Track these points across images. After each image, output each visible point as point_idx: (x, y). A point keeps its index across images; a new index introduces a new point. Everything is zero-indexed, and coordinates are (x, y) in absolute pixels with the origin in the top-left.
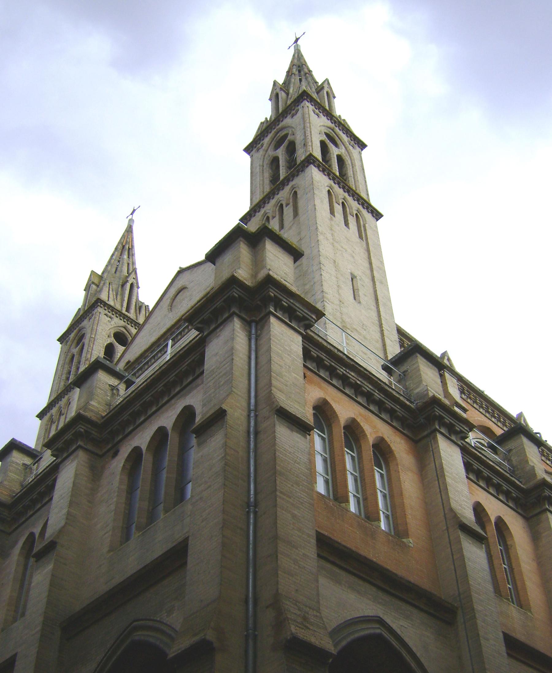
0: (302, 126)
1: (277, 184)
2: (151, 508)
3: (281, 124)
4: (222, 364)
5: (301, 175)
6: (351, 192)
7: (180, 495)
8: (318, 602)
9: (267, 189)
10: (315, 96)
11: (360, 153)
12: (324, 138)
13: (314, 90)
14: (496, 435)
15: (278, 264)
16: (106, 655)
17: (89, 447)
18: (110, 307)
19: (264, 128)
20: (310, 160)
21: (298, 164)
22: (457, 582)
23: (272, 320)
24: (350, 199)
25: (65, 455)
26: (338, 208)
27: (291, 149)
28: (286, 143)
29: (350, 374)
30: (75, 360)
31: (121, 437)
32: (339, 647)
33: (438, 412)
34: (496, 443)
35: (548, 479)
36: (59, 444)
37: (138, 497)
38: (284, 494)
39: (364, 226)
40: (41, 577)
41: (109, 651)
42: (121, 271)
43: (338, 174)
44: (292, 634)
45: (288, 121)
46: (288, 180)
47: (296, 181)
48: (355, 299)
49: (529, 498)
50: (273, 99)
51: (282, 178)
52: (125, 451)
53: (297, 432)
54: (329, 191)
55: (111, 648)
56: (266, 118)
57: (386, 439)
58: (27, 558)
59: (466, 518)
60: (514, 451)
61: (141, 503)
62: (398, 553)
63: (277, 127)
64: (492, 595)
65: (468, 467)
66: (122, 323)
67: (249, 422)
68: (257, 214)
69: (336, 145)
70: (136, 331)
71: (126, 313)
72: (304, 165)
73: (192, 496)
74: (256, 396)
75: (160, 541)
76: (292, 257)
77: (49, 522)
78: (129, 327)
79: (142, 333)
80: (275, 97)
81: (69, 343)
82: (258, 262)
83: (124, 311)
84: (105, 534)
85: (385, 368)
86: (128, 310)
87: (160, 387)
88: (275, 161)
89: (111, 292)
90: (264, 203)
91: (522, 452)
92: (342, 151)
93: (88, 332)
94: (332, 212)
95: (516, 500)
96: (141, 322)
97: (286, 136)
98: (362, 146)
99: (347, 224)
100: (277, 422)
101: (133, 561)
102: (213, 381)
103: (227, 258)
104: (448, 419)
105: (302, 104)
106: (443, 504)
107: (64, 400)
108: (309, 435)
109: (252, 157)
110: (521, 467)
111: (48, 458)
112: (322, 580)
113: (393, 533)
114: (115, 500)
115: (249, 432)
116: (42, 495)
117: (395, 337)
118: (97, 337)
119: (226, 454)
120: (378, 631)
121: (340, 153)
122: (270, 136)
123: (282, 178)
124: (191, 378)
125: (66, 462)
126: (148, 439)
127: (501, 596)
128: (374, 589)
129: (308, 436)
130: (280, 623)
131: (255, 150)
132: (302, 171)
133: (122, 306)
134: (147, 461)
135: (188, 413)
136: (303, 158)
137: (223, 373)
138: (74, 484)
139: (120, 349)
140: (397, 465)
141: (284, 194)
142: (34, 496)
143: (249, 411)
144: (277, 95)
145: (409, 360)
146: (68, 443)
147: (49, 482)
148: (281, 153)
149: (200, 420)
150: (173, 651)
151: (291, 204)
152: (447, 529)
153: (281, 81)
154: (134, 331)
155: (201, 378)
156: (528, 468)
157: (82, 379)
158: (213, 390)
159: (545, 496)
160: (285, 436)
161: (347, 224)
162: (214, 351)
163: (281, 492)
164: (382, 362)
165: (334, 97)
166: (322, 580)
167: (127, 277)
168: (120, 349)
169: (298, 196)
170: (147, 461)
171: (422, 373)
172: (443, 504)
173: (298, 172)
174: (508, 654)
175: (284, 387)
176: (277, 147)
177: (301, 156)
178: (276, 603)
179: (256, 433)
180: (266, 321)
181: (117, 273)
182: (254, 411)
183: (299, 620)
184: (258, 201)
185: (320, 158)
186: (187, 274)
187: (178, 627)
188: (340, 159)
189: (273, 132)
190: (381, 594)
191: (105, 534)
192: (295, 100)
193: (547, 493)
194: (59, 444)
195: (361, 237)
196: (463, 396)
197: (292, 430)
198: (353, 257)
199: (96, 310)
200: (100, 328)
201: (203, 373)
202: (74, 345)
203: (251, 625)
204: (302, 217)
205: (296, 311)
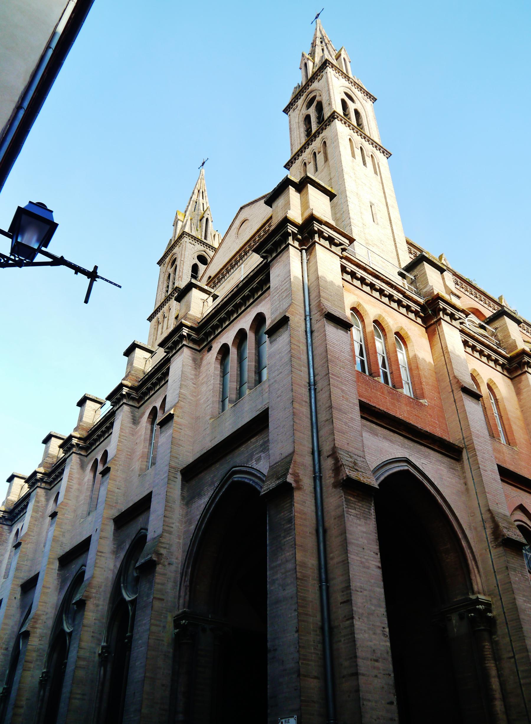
0: (327, 88)
1: (311, 137)
2: (238, 387)
3: (311, 88)
4: (283, 283)
5: (328, 128)
6: (367, 138)
7: (259, 380)
8: (364, 451)
9: (303, 141)
10: (335, 62)
13: (334, 57)
14: (484, 316)
15: (320, 205)
16: (214, 492)
17: (191, 345)
18: (192, 237)
19: (297, 92)
20: (333, 116)
21: (325, 119)
22: (462, 429)
23: (317, 246)
25: (174, 352)
26: (358, 152)
27: (320, 108)
28: (315, 103)
30: (171, 278)
31: (212, 337)
32: (379, 481)
33: (442, 305)
34: (485, 323)
35: (527, 349)
36: (170, 344)
37: (229, 379)
38: (335, 376)
39: (378, 164)
40: (164, 438)
41: (216, 488)
42: (199, 209)
43: (356, 125)
44: (347, 476)
45: (315, 85)
46: (318, 133)
47: (325, 133)
49: (513, 365)
51: (313, 132)
52: (216, 346)
53: (341, 329)
54: (350, 139)
55: (218, 487)
57: (404, 328)
58: (152, 423)
59: (465, 382)
60: (499, 329)
61: (232, 384)
62: (417, 410)
63: (307, 91)
64: (488, 437)
65: (465, 343)
66: (202, 248)
67: (306, 324)
68: (297, 161)
70: (214, 253)
71: (205, 241)
72: (330, 120)
73: (269, 380)
74: (310, 305)
75: (247, 413)
77: (167, 400)
78: (208, 251)
79: (217, 255)
81: (166, 265)
82: (305, 204)
83: (203, 240)
84: (207, 406)
85: (401, 274)
86: (205, 238)
88: (308, 118)
89: (192, 225)
90: (302, 152)
91: (505, 329)
93: (178, 256)
94: (353, 156)
95: (503, 366)
96: (217, 247)
97: (314, 97)
99: (365, 164)
100: (326, 324)
101: (229, 426)
102: (278, 295)
103: (280, 202)
104: (450, 310)
105: (325, 71)
106: (448, 373)
107: (166, 308)
108: (350, 331)
110: (504, 341)
111: (161, 353)
112: (365, 434)
113: (412, 397)
114: (212, 382)
115: (306, 331)
116: (159, 380)
117: (405, 246)
118: (186, 259)
119: (291, 349)
120: (406, 468)
122: (303, 98)
123: (313, 132)
124: (260, 293)
125: (175, 356)
126: (233, 338)
127: (494, 437)
128: (402, 438)
129: (349, 332)
130: (337, 468)
131: (291, 110)
132: (329, 125)
133: (201, 236)
134: (233, 352)
135: (260, 319)
136: (329, 114)
137: (284, 289)
138: (182, 372)
139: (202, 267)
140: (413, 346)
141: (316, 144)
142: (154, 380)
143: (306, 316)
145: (418, 267)
146: (176, 343)
147: (164, 370)
148: (312, 111)
149: (271, 323)
150: (264, 489)
151: (322, 152)
152: (452, 391)
154: (211, 253)
155: (267, 292)
156: (511, 341)
157: (182, 294)
158: (278, 302)
159: (525, 362)
160: (333, 333)
161: (365, 164)
162: (276, 274)
163: (333, 374)
164: (398, 270)
166: (365, 434)
167: (204, 213)
168: (202, 267)
169: (327, 145)
170: (233, 352)
171: (428, 276)
172: (448, 373)
173: (326, 126)
174: (502, 480)
175: (330, 297)
176: (309, 106)
177: (327, 114)
178: (334, 454)
179: (312, 332)
180: (313, 249)
181: (196, 210)
182: (308, 317)
183: (351, 465)
184: (297, 150)
185: (342, 114)
186: (246, 209)
187: (265, 471)
188: (357, 112)
189: (304, 95)
190: (406, 441)
191: (207, 406)
192: (320, 68)
193: (526, 359)
194: (170, 344)
195: (376, 173)
196: (457, 286)
197: (337, 328)
198: (371, 189)
199: (183, 240)
200: (187, 253)
201: (269, 287)
202: (169, 267)
203: (317, 470)
204: (331, 161)
205: (334, 239)
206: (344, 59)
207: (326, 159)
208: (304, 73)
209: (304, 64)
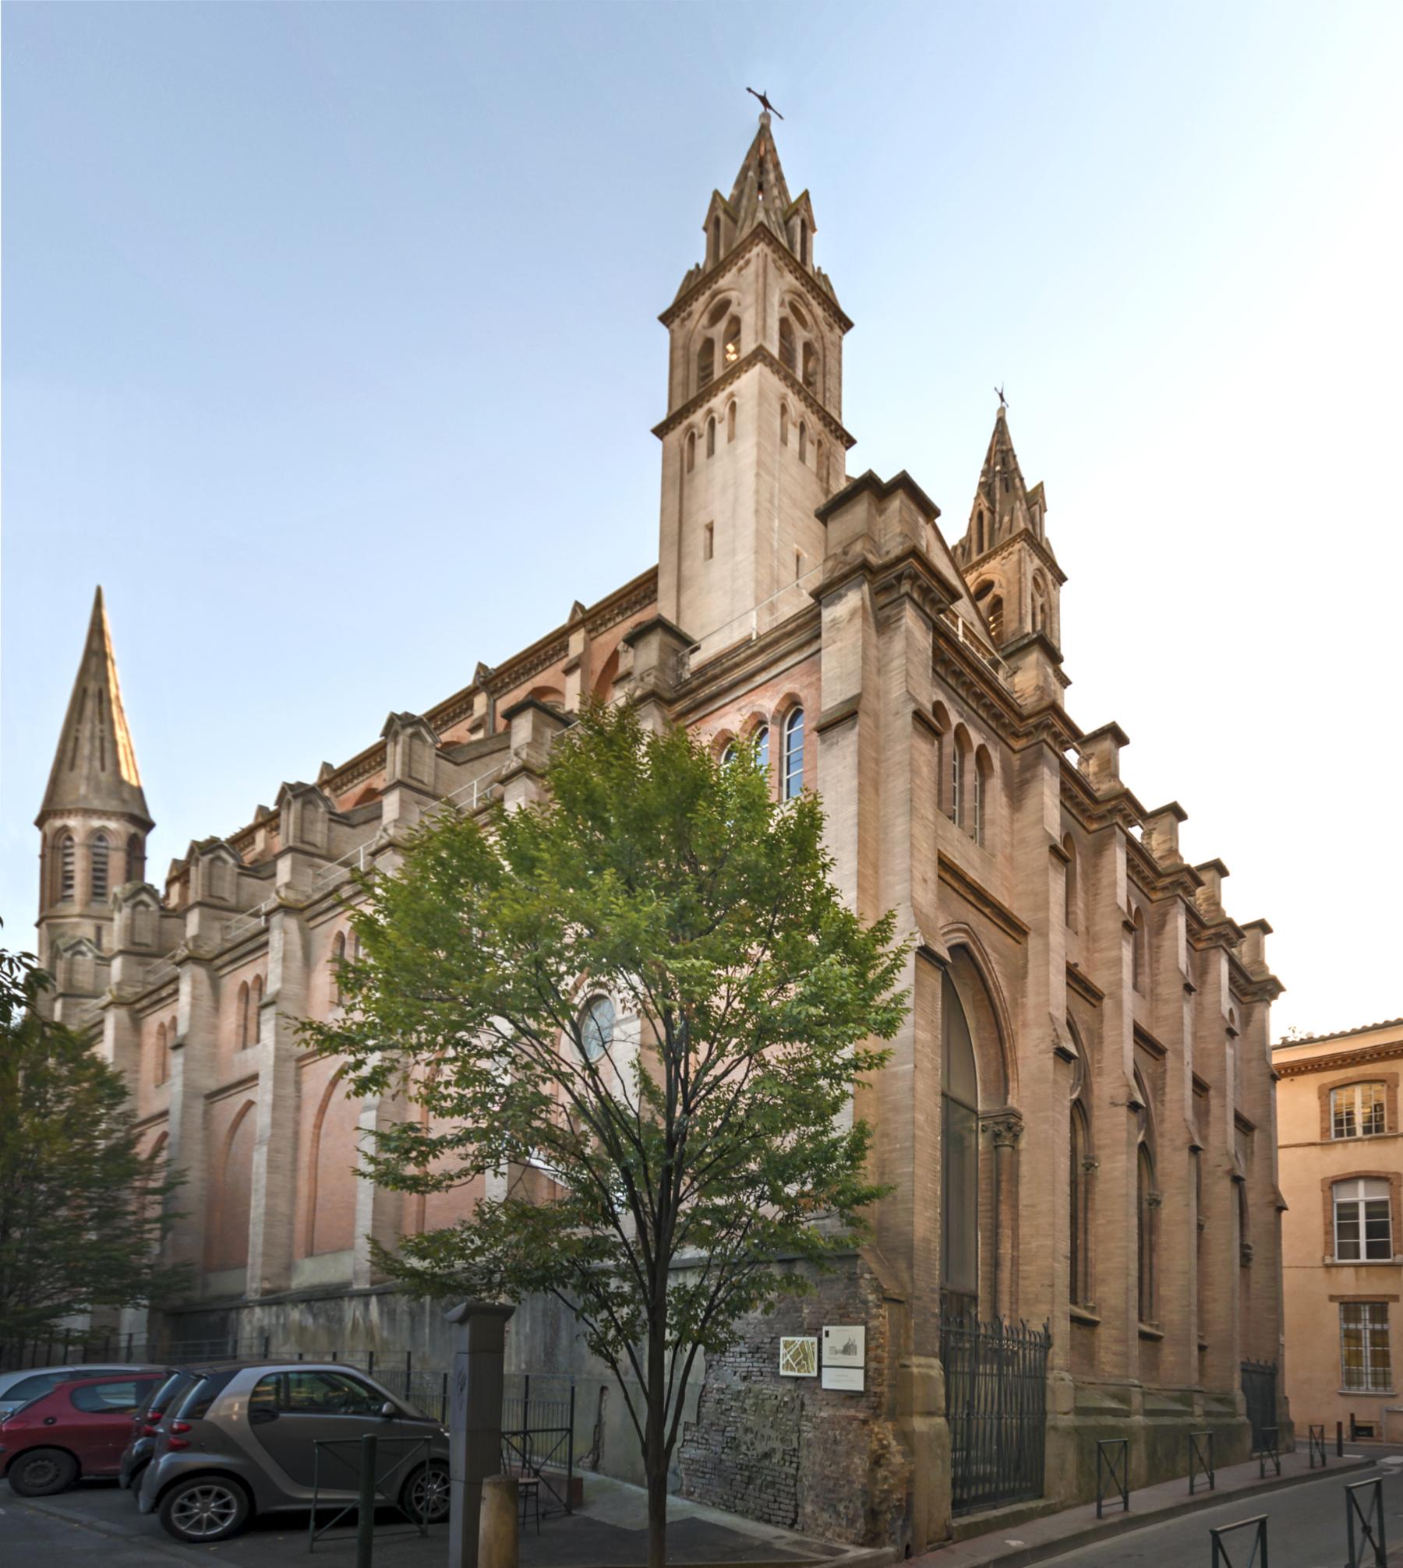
11: (840, 338)
12: (787, 311)
19: (693, 284)
29: (811, 312)
48: (1067, 924)
50: (711, 227)
56: (697, 266)
80: (713, 225)
87: (71, 745)
98: (846, 324)
109: (672, 332)
144: (717, 222)
153: (727, 193)
165: (814, 230)
176: (715, 318)
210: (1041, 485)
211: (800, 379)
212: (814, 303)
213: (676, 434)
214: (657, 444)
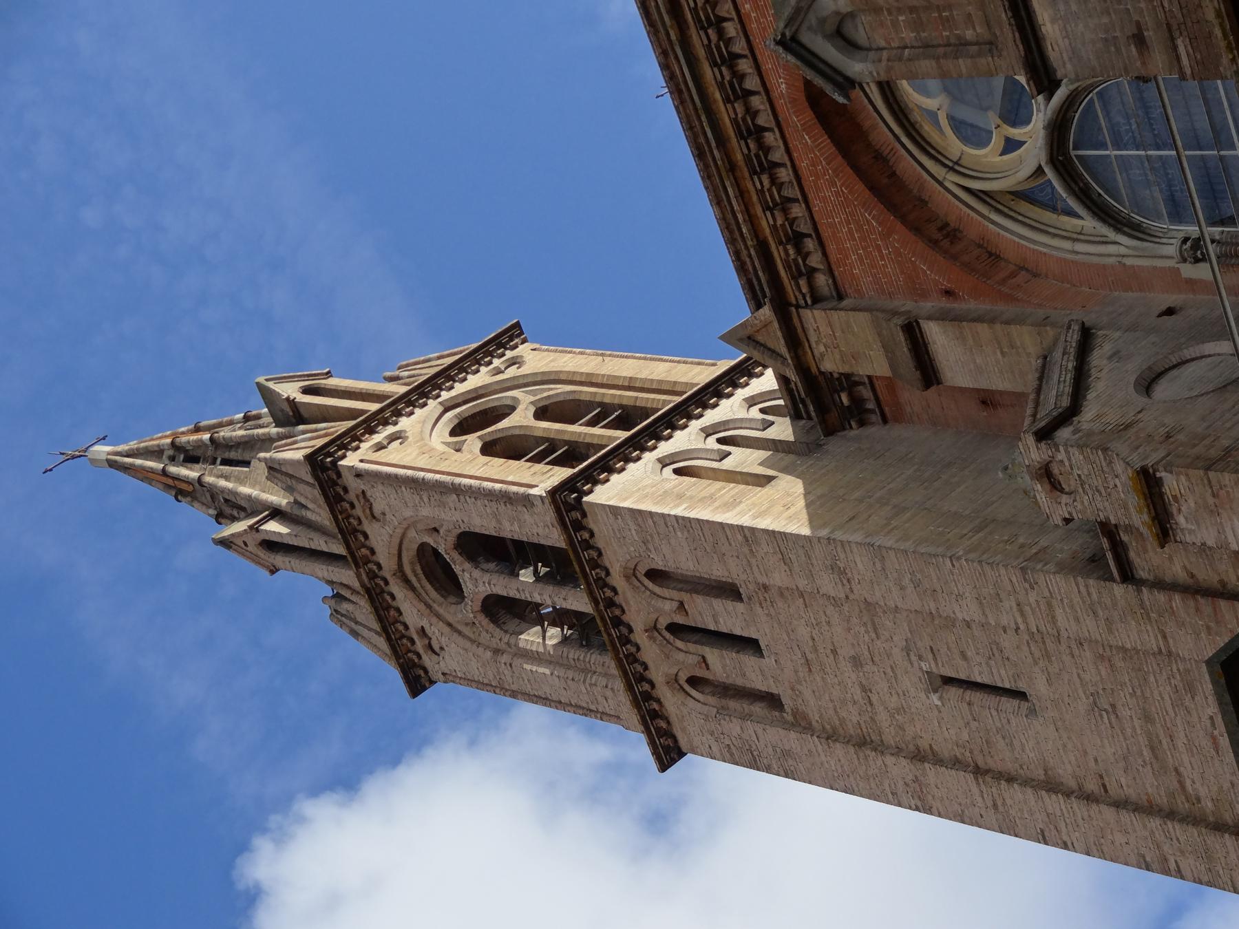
12: (473, 442)
20: (567, 501)
24: (711, 417)
45: (381, 538)
47: (616, 558)
54: (677, 472)
69: (507, 410)
76: (238, 861)
90: (642, 679)
92: (525, 401)
121: (532, 409)
141: (642, 609)
148: (480, 582)
151: (685, 597)
176: (449, 584)
185: (562, 474)
206: (361, 461)
207: (730, 591)
208: (295, 562)
209: (262, 554)
210: (723, 338)
211: (622, 435)
212: (459, 388)
213: (688, 714)
214: (691, 764)
